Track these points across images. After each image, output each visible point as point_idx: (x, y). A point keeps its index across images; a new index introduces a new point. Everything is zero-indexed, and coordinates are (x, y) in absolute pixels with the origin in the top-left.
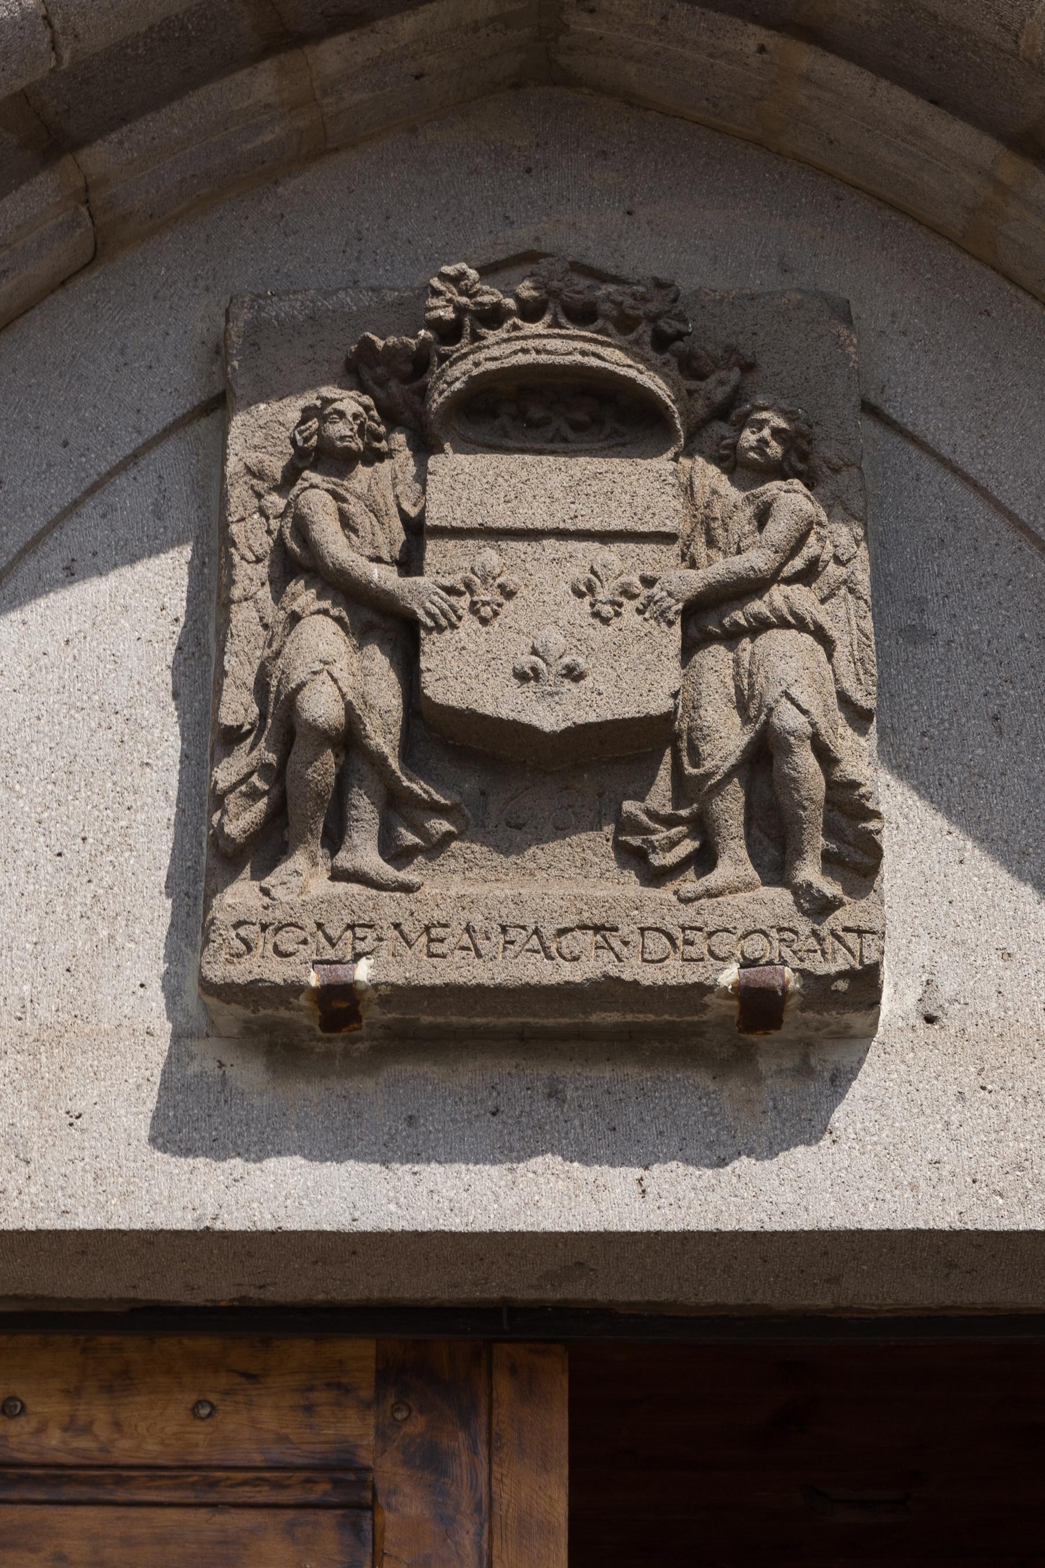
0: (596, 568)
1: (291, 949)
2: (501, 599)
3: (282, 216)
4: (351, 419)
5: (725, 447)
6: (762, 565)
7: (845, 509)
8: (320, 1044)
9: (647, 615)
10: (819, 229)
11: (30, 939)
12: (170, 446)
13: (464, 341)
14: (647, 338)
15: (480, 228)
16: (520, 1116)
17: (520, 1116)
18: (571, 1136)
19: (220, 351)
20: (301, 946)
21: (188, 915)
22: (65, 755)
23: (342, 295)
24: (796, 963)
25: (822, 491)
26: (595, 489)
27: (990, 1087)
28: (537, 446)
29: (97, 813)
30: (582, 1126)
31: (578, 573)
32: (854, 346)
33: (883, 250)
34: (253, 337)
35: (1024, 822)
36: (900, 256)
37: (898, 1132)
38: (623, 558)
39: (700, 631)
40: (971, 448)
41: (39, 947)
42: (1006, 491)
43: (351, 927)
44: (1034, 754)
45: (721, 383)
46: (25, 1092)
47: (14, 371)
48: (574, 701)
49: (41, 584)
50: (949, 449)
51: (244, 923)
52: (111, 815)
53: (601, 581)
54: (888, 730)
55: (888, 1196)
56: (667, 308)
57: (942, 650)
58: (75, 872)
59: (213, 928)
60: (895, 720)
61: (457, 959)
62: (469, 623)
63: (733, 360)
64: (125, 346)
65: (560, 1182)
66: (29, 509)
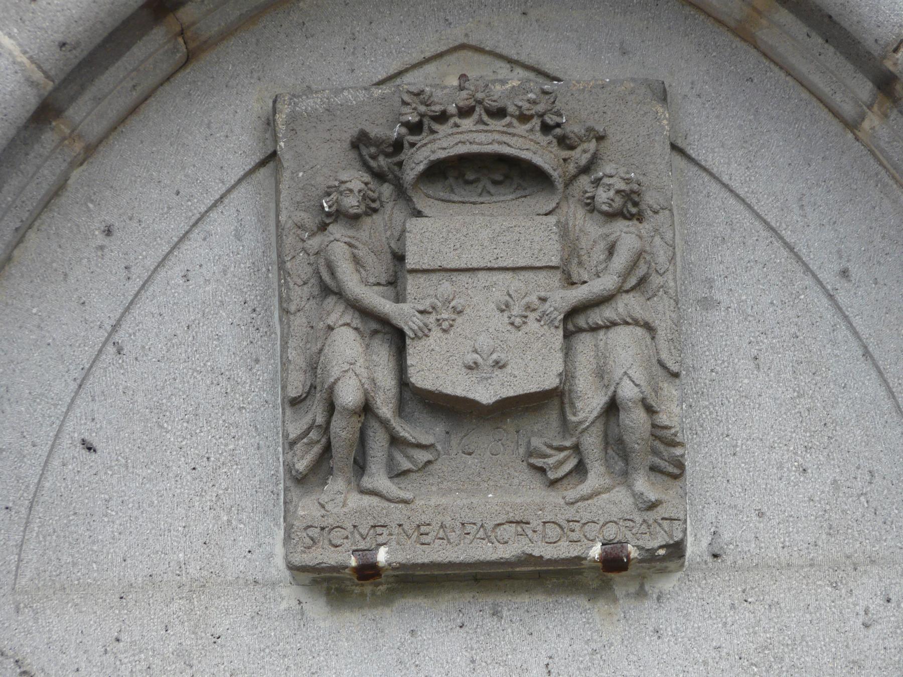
0: (511, 292)
1: (339, 543)
2: (453, 316)
3: (304, 23)
4: (357, 194)
5: (588, 198)
6: (611, 286)
7: (662, 238)
8: (357, 588)
9: (542, 323)
10: (645, 22)
11: (181, 524)
12: (242, 188)
13: (424, 134)
14: (538, 128)
15: (430, 29)
16: (477, 628)
17: (477, 628)
18: (507, 639)
19: (270, 123)
20: (345, 541)
21: (274, 506)
22: (193, 403)
23: (346, 93)
24: (635, 542)
25: (647, 226)
26: (508, 238)
27: (750, 600)
28: (472, 200)
29: (214, 441)
30: (513, 633)
31: (499, 295)
32: (666, 119)
33: (685, 36)
34: (292, 125)
35: (772, 427)
36: (696, 40)
37: (696, 630)
38: (527, 283)
39: (574, 326)
40: (741, 177)
41: (187, 529)
42: (762, 206)
43: (374, 527)
44: (778, 382)
45: (585, 151)
46: (186, 624)
47: (142, 142)
48: (500, 383)
49: (169, 288)
50: (727, 177)
51: (311, 526)
52: (223, 442)
53: (514, 301)
54: (690, 369)
55: (691, 669)
56: (549, 108)
57: (723, 313)
58: (205, 480)
59: (293, 530)
60: (695, 362)
61: (436, 546)
62: (436, 333)
63: (591, 135)
64: (210, 122)
65: (501, 668)
66: (158, 239)
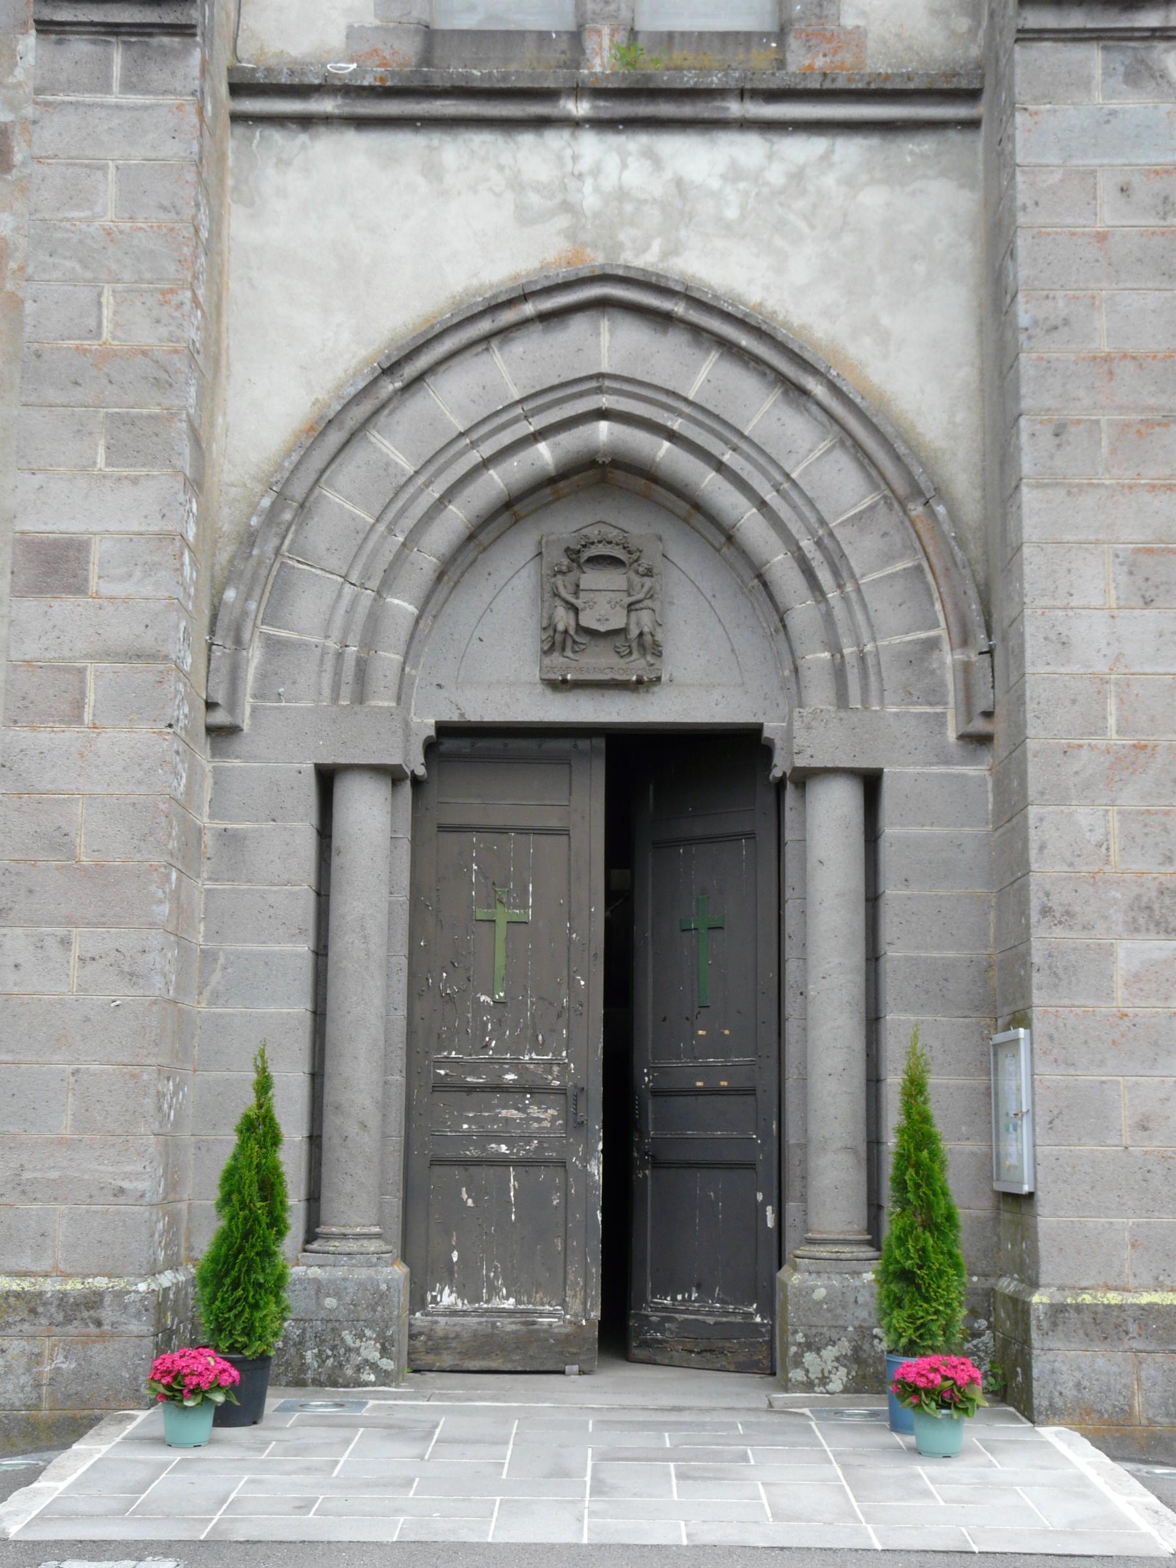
19: (540, 543)
